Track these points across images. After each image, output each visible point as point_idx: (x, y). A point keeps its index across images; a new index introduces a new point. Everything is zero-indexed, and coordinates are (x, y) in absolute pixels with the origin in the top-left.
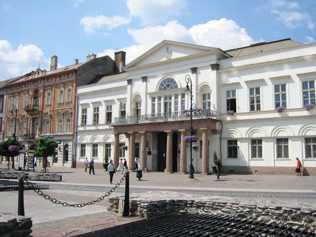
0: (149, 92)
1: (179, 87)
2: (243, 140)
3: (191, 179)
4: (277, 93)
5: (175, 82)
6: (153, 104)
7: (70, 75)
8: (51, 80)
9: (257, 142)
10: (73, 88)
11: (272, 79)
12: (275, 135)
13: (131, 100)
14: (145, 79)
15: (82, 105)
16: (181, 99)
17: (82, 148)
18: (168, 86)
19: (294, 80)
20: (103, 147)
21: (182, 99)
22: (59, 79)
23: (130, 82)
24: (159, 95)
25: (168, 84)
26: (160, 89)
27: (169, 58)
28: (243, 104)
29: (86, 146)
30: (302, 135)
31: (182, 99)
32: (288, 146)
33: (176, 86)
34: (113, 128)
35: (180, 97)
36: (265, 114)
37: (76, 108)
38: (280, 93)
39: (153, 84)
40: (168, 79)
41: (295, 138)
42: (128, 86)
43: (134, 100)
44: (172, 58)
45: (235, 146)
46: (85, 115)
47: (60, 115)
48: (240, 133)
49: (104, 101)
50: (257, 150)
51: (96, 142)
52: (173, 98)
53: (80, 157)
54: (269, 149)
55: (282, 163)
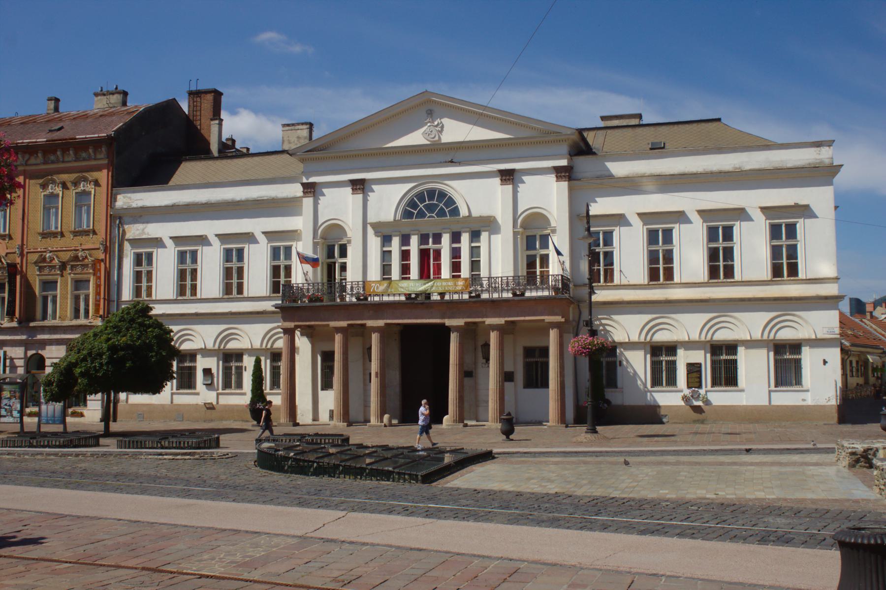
0: (372, 218)
1: (463, 212)
2: (631, 346)
3: (589, 436)
5: (451, 202)
6: (384, 252)
8: (92, 154)
10: (66, 191)
12: (772, 337)
13: (314, 238)
14: (359, 186)
15: (135, 242)
20: (215, 359)
23: (310, 189)
24: (406, 231)
26: (407, 214)
27: (437, 138)
28: (210, 281)
31: (473, 245)
32: (800, 359)
33: (455, 212)
35: (396, 241)
37: (112, 247)
38: (784, 242)
39: (387, 201)
40: (431, 193)
41: (751, 344)
42: (305, 200)
43: (323, 237)
45: (729, 357)
46: (725, 249)
47: (50, 266)
48: (624, 329)
51: (232, 345)
52: (446, 239)
53: (175, 390)
54: (755, 368)
55: (786, 398)
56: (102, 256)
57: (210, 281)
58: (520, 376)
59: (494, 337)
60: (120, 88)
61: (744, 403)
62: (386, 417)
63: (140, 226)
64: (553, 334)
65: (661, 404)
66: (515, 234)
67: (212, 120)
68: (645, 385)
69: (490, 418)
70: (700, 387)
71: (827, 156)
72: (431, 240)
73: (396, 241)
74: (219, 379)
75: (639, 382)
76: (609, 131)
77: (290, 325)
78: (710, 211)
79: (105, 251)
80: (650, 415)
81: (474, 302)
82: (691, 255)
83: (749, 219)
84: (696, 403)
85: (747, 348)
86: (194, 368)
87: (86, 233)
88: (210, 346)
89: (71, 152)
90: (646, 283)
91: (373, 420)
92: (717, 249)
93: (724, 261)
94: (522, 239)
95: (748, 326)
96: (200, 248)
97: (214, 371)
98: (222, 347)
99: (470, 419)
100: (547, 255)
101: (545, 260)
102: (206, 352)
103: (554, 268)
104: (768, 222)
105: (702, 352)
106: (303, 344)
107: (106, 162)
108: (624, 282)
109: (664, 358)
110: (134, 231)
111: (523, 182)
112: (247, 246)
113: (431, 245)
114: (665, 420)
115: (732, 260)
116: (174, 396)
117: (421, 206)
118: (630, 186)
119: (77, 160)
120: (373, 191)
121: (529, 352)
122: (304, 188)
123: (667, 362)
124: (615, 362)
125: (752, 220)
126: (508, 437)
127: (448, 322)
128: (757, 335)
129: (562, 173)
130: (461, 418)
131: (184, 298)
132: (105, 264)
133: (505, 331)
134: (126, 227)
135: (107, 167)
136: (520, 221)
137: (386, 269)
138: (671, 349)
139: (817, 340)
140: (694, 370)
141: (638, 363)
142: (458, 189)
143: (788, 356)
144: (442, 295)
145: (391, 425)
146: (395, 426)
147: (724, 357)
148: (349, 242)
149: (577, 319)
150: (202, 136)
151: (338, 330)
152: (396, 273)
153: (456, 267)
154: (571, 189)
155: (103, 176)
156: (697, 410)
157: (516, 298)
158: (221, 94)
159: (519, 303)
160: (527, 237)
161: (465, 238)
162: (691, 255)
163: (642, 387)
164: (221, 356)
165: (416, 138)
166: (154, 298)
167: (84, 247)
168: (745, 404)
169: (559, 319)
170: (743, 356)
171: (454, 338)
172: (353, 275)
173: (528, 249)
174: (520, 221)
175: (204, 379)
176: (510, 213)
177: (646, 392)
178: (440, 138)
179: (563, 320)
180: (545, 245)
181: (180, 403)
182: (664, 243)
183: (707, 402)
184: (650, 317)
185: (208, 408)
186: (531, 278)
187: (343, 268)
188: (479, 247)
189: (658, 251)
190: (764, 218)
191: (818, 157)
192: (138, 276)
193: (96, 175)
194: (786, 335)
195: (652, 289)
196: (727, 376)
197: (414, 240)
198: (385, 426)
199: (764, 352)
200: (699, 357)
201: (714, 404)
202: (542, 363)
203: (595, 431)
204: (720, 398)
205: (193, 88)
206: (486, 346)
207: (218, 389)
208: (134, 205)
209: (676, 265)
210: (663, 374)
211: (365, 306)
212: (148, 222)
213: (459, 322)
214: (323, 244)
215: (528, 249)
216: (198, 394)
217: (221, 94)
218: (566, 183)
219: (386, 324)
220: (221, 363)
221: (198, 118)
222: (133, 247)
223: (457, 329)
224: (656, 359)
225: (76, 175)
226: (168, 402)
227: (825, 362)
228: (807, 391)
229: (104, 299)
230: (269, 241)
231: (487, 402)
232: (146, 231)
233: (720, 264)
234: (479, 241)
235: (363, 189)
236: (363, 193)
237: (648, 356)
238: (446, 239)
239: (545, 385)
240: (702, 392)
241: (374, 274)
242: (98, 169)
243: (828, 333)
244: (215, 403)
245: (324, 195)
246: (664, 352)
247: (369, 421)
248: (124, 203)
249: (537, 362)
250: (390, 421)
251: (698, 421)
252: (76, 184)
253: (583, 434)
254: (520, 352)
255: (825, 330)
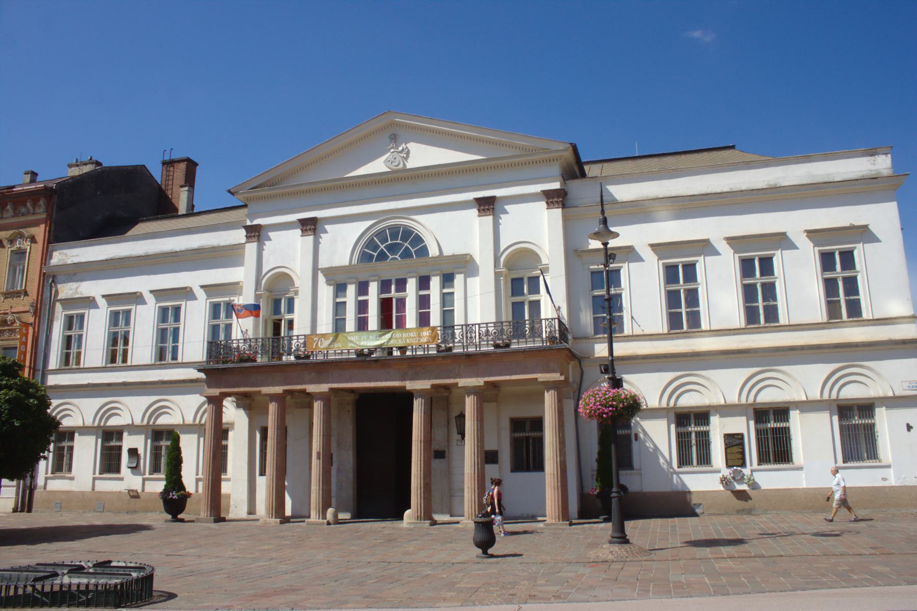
0: (323, 263)
1: (433, 251)
3: (616, 548)
4: (215, 322)
5: (418, 239)
7: (25, 206)
8: (31, 208)
9: (528, 427)
10: (33, 245)
11: (813, 235)
12: (102, 424)
13: (256, 290)
14: (310, 226)
15: (68, 303)
16: (356, 298)
17: (156, 444)
18: (392, 248)
19: (147, 300)
20: (143, 437)
21: (445, 291)
22: (11, 213)
23: (255, 233)
24: (363, 278)
25: (394, 247)
26: (365, 257)
27: (401, 166)
29: (76, 435)
30: (668, 404)
31: (445, 291)
33: (424, 251)
34: (202, 376)
35: (351, 290)
36: (859, 326)
37: (42, 310)
38: (758, 279)
39: (342, 243)
40: (394, 231)
41: (808, 406)
42: (247, 245)
43: (269, 290)
44: (410, 164)
46: (764, 285)
48: (647, 387)
49: (103, 296)
50: (694, 442)
51: (113, 422)
52: (412, 285)
53: (49, 475)
54: (814, 440)
55: (860, 477)
56: (32, 320)
57: (142, 346)
58: (506, 457)
59: (470, 404)
60: (94, 159)
61: (804, 485)
62: (330, 511)
63: (73, 285)
64: (549, 398)
65: (692, 489)
66: (497, 275)
67: (181, 187)
68: (670, 464)
69: (466, 514)
70: (743, 465)
71: (885, 166)
72: (393, 287)
73: (351, 290)
74: (146, 462)
75: (662, 460)
76: (605, 165)
77: (216, 392)
78: (743, 237)
79: (35, 313)
80: (679, 505)
81: (443, 357)
82: (721, 294)
83: (792, 246)
84: (739, 487)
85: (802, 411)
86: (120, 448)
87: (17, 294)
88: (138, 421)
89: (9, 207)
90: (666, 331)
91: (314, 517)
92: (754, 286)
93: (764, 301)
94: (506, 283)
95: (803, 382)
96: (133, 307)
97: (141, 451)
98: (102, 424)
99: (442, 512)
100: (538, 302)
101: (535, 306)
102: (133, 429)
103: (547, 311)
104: (817, 249)
105: (744, 419)
106: (232, 413)
107: (44, 216)
108: (638, 331)
109: (693, 428)
110: (66, 290)
111: (506, 212)
112: (183, 303)
113: (393, 293)
114: (698, 511)
115: (775, 299)
116: (97, 482)
117: (382, 247)
118: (640, 212)
119: (16, 215)
120: (326, 232)
121: (517, 424)
122: (247, 232)
123: (697, 433)
124: (629, 436)
125: (796, 248)
126: (485, 552)
127: (410, 385)
128: (815, 395)
129: (554, 198)
130: (427, 514)
131: (114, 365)
132: (34, 329)
133: (488, 395)
134: (59, 286)
135: (45, 221)
136: (502, 259)
137: (339, 325)
138: (702, 416)
139: (895, 398)
140: (734, 442)
141: (658, 435)
142: (427, 224)
143: (856, 421)
144: (403, 349)
145: (337, 522)
146: (344, 522)
147: (772, 425)
148: (296, 293)
149: (578, 380)
150: (173, 204)
151: (273, 397)
152: (350, 324)
153: (424, 320)
154: (566, 220)
155: (40, 232)
156: (742, 496)
157: (499, 350)
158: (196, 164)
159: (501, 355)
160: (513, 280)
161: (435, 282)
162: (721, 294)
163: (665, 467)
164: (150, 433)
165: (378, 166)
166: (82, 366)
167: (13, 310)
168: (805, 486)
169: (556, 377)
170: (797, 422)
171: (418, 407)
172: (301, 327)
173: (513, 294)
174: (502, 259)
175: (129, 462)
176: (489, 248)
177: (672, 474)
178: (404, 165)
179: (562, 378)
180: (535, 289)
181: (102, 490)
182: (686, 280)
183: (754, 486)
184: (671, 375)
185: (132, 497)
186: (518, 329)
187: (291, 323)
188: (453, 293)
189: (679, 291)
190: (812, 245)
191: (873, 168)
192: (68, 341)
193: (33, 231)
194: (852, 392)
195: (673, 339)
196: (777, 449)
197: (373, 288)
198: (329, 523)
199: (825, 416)
200: (741, 425)
201: (763, 488)
202: (534, 438)
203: (622, 538)
204: (771, 479)
205: (167, 158)
206: (462, 416)
207: (144, 474)
208: (69, 262)
209: (702, 308)
210: (693, 450)
211: (312, 366)
212: (82, 280)
213: (423, 384)
214: (268, 298)
215: (513, 294)
216: (122, 479)
217: (196, 164)
218: (560, 210)
219: (331, 389)
220: (149, 441)
221: (170, 187)
222: (65, 308)
223: (422, 393)
224: (682, 430)
225: (11, 232)
226: (88, 488)
227: (909, 428)
228: (889, 467)
229: (30, 367)
230: (209, 296)
231: (463, 490)
232: (79, 290)
233: (760, 303)
234: (452, 286)
235: (315, 230)
236: (315, 234)
237: (673, 426)
238: (412, 285)
239: (538, 465)
240: (746, 471)
241: (325, 325)
242: (36, 224)
243: (910, 388)
244: (140, 490)
245: (270, 239)
246: (693, 421)
247: (309, 517)
248: (59, 260)
249: (527, 438)
250: (335, 516)
251: (743, 510)
252: (12, 241)
253: (606, 546)
254: (506, 425)
255: (905, 385)
